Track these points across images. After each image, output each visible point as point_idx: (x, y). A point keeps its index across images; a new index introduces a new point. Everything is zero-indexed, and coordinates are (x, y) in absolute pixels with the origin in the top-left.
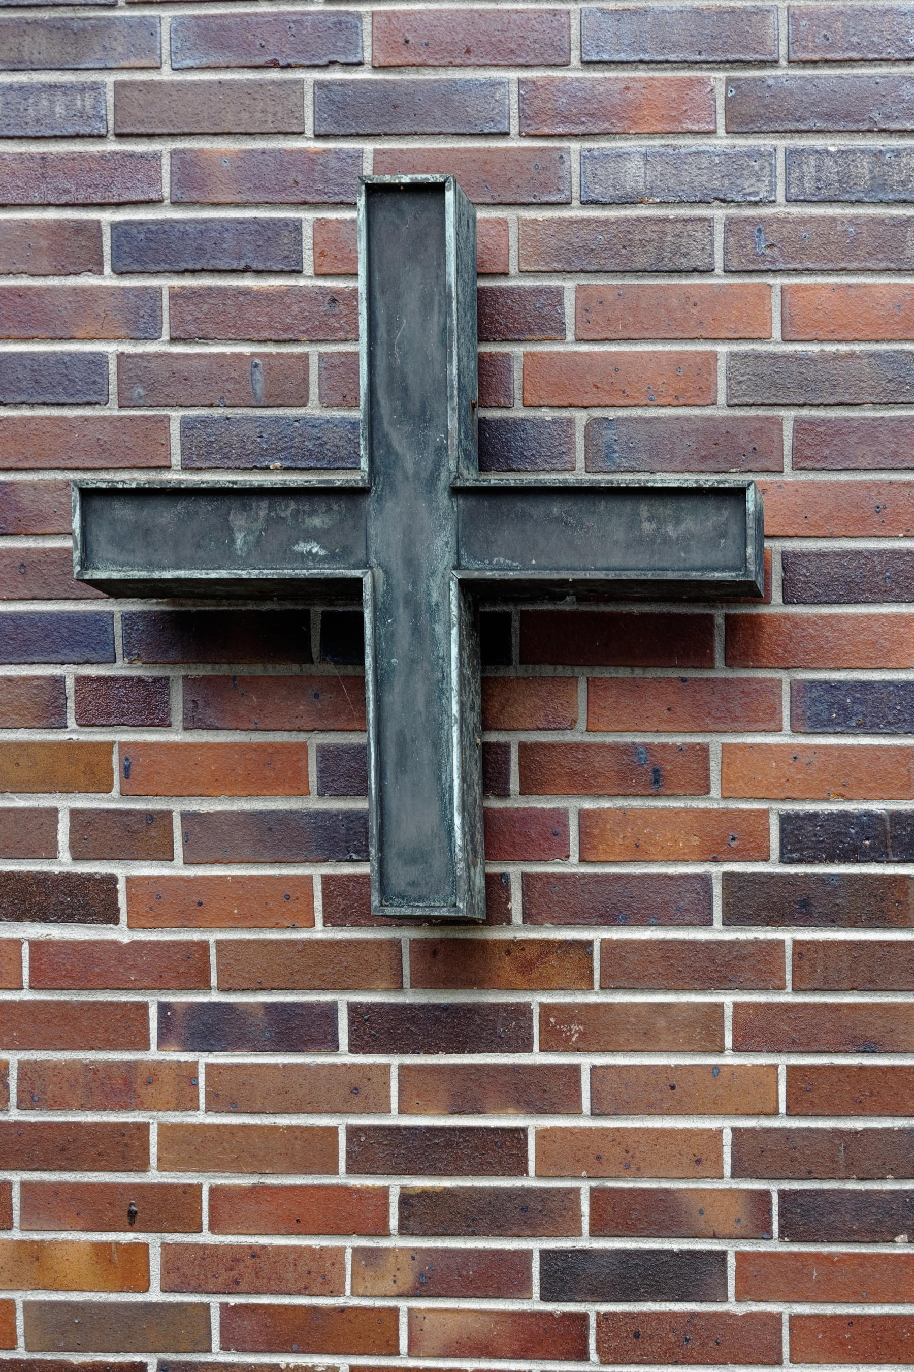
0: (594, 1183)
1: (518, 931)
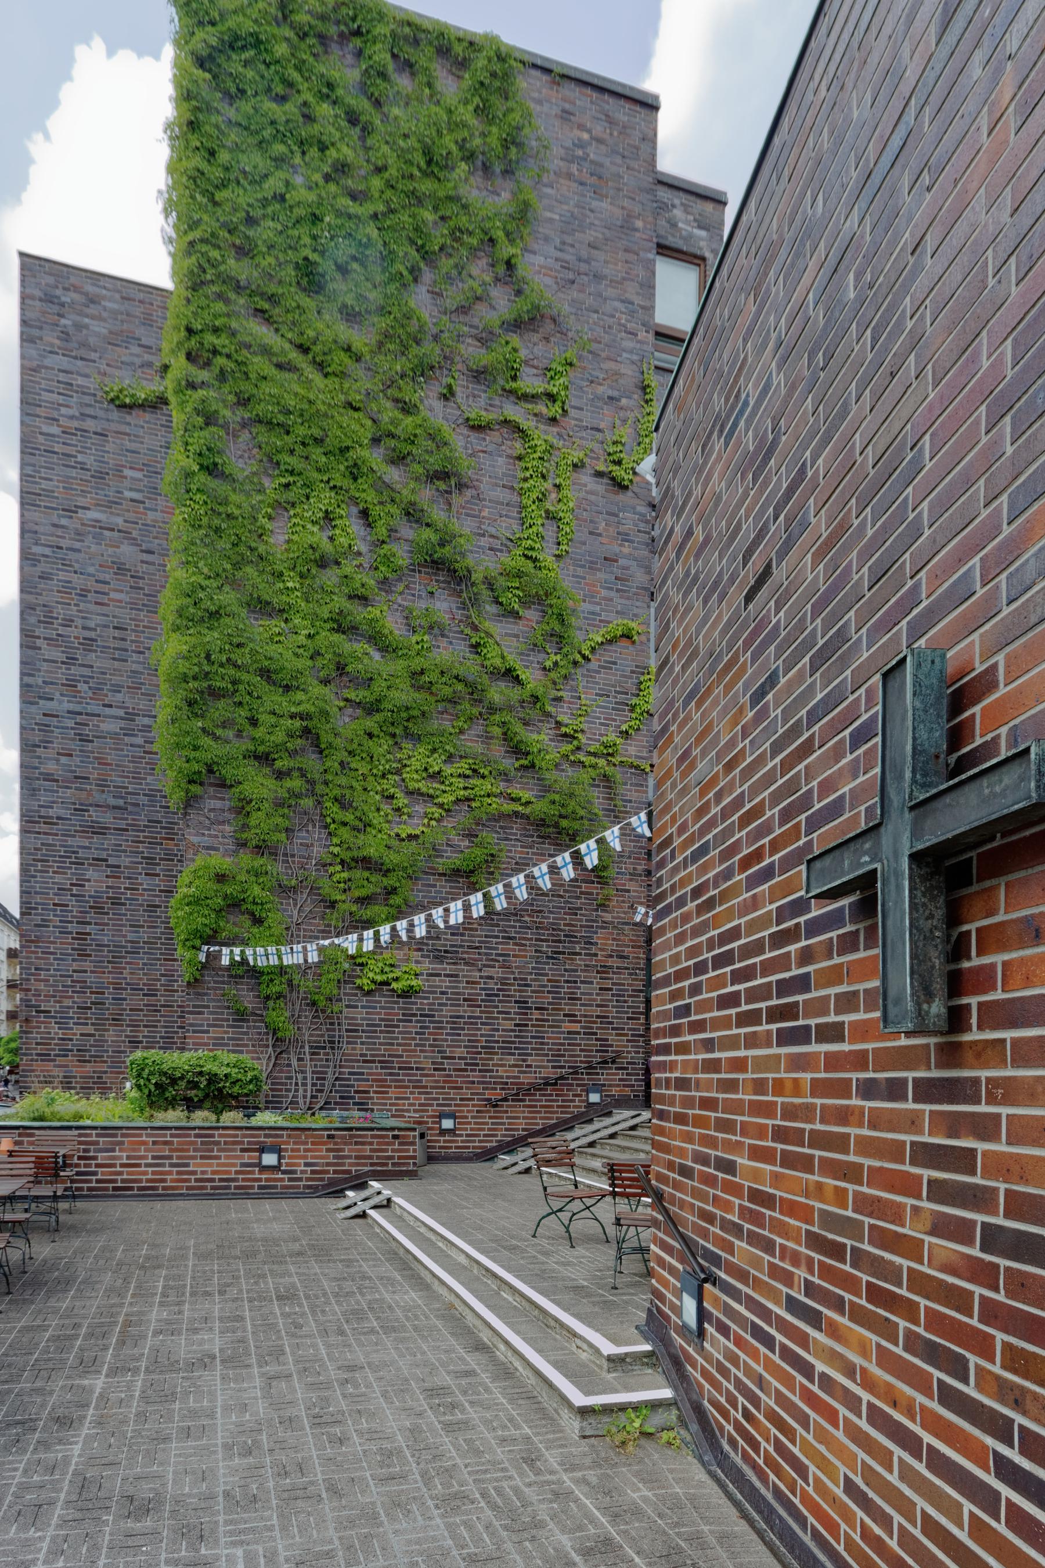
0: (1007, 1186)
1: (974, 1035)
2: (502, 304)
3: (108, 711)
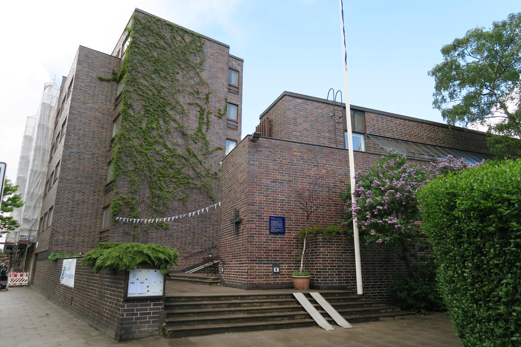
2: (197, 80)
3: (87, 152)
